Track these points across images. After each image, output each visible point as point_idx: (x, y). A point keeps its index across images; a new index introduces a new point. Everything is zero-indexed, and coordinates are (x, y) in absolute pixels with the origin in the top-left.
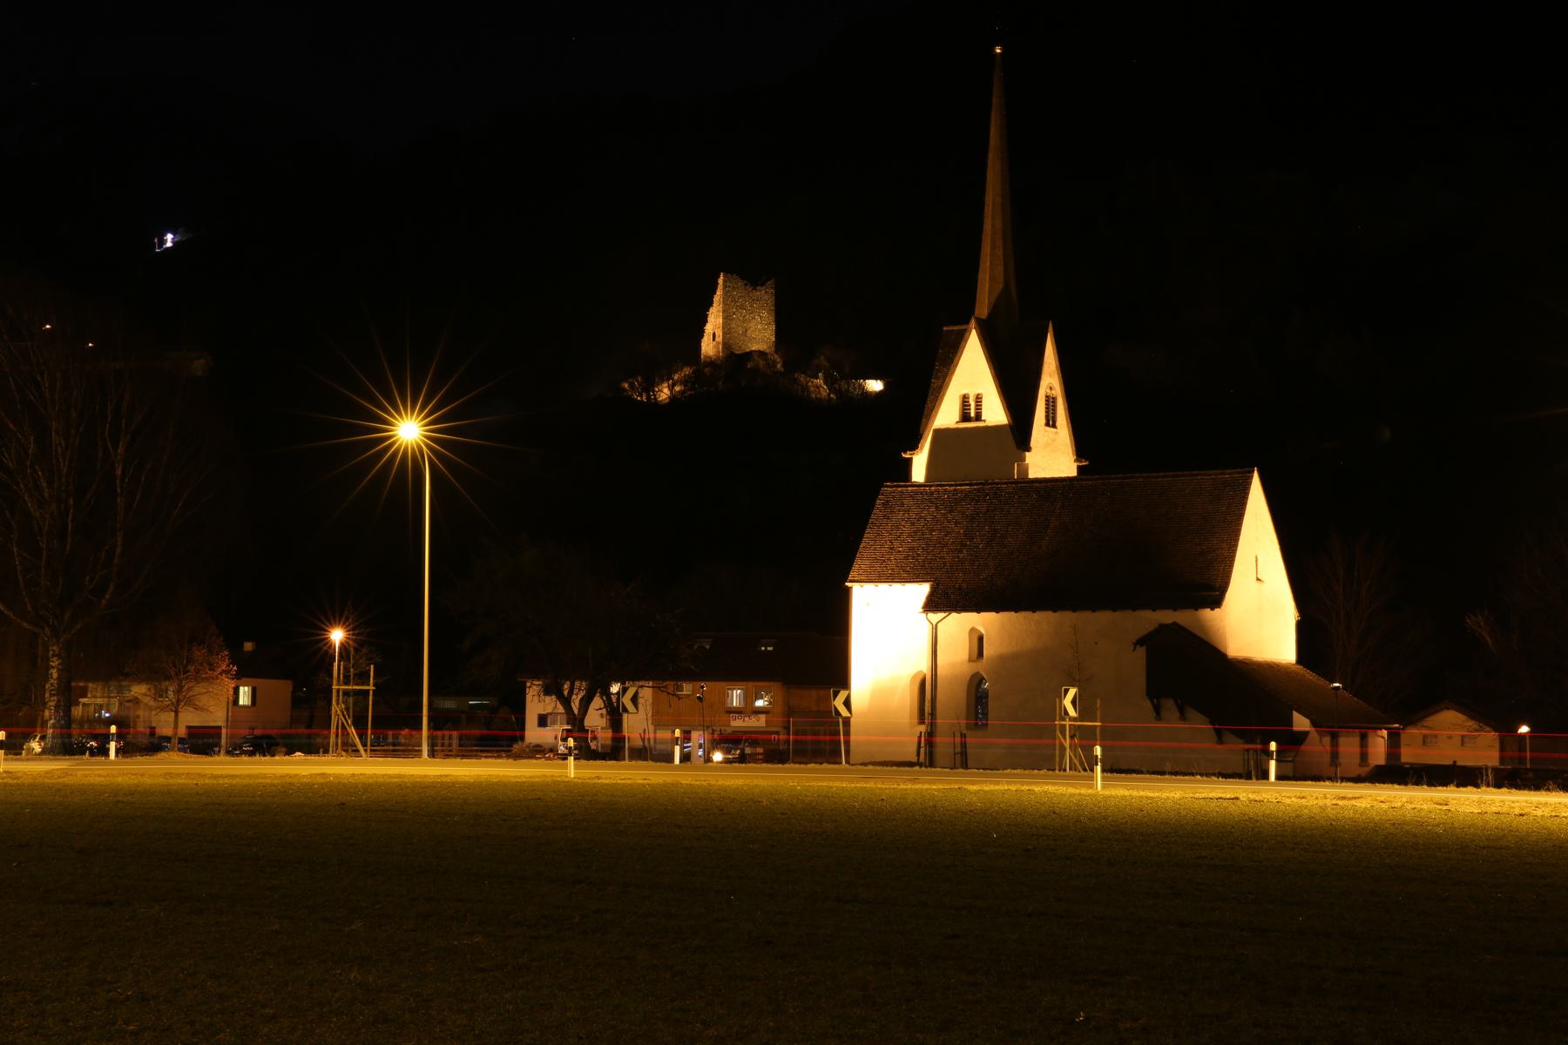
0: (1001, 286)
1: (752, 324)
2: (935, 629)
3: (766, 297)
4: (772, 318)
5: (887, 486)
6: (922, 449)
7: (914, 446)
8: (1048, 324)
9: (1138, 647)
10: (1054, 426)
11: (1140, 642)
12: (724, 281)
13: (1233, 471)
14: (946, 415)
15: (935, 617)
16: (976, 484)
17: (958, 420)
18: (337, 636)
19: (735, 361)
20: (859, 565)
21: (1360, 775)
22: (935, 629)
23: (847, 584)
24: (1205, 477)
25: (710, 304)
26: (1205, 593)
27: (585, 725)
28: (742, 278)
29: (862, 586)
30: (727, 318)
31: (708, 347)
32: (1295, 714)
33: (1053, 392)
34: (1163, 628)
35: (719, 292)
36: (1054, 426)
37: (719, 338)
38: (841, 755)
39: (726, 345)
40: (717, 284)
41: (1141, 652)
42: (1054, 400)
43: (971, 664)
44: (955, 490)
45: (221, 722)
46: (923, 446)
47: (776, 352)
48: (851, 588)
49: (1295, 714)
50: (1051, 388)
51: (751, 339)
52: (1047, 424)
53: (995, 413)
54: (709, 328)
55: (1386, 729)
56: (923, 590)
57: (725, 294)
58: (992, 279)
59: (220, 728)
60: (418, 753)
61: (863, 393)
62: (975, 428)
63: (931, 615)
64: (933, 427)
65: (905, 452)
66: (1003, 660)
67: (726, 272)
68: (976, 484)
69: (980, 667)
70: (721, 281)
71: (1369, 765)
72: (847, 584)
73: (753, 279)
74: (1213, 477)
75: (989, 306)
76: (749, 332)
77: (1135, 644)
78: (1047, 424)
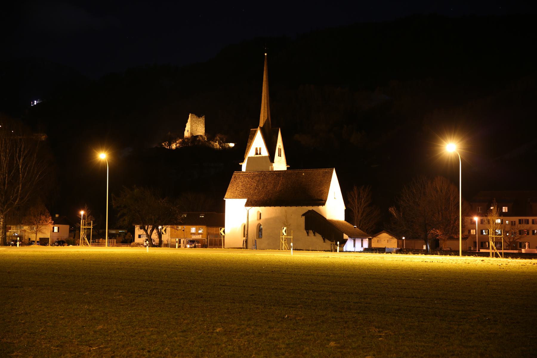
0: (266, 118)
3: (202, 120)
4: (204, 126)
7: (242, 161)
9: (303, 216)
10: (280, 156)
11: (303, 215)
12: (191, 116)
14: (251, 153)
19: (194, 138)
25: (187, 122)
28: (196, 115)
30: (192, 126)
31: (187, 134)
32: (344, 234)
36: (280, 156)
37: (189, 131)
39: (191, 133)
44: (254, 173)
47: (205, 135)
49: (344, 234)
51: (198, 132)
52: (279, 156)
53: (265, 153)
54: (187, 129)
55: (368, 238)
57: (191, 119)
58: (264, 116)
59: (49, 238)
65: (240, 163)
66: (267, 220)
67: (191, 113)
69: (261, 222)
70: (190, 116)
73: (199, 116)
75: (263, 123)
77: (302, 216)
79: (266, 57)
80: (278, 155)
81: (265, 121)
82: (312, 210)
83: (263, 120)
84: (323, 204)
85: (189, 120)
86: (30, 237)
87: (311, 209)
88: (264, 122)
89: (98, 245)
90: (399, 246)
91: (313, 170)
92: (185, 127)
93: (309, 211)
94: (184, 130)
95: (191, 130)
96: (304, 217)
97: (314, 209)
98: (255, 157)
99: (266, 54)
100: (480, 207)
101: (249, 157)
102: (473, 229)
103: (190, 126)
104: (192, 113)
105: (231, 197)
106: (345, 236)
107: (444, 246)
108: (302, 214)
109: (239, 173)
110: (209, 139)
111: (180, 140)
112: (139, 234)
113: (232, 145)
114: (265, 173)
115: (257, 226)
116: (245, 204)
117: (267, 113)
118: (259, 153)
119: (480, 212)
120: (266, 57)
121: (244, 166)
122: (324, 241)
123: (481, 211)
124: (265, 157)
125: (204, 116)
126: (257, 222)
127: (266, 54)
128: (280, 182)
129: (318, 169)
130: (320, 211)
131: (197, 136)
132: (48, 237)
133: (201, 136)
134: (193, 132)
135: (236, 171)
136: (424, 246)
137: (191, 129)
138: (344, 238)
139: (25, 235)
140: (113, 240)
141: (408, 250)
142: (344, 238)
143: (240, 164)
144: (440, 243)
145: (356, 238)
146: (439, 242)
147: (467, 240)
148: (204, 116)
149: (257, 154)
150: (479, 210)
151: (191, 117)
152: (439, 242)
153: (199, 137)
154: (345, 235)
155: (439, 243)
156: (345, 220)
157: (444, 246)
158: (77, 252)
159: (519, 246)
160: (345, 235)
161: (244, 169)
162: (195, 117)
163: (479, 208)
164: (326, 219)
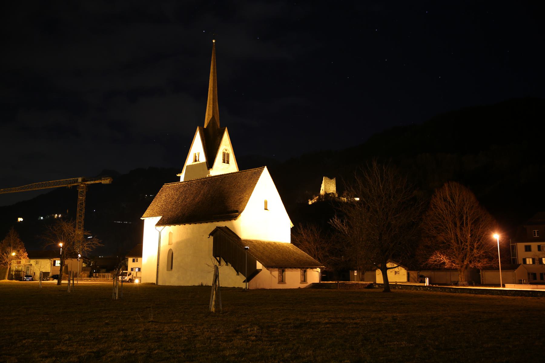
0: (211, 117)
1: (331, 187)
2: (160, 233)
3: (334, 181)
4: (335, 186)
5: (165, 185)
7: (180, 172)
8: (225, 129)
9: (211, 236)
10: (228, 163)
11: (211, 234)
12: (324, 178)
13: (254, 169)
14: (190, 161)
16: (187, 181)
18: (61, 245)
19: (327, 195)
20: (148, 211)
21: (300, 287)
22: (160, 233)
23: (141, 218)
24: (250, 171)
25: (322, 183)
26: (234, 214)
27: (389, 281)
28: (328, 178)
30: (325, 186)
31: (322, 192)
32: (258, 262)
36: (228, 163)
37: (324, 190)
39: (326, 192)
40: (323, 179)
41: (212, 238)
42: (228, 155)
43: (169, 245)
44: (181, 184)
45: (50, 271)
47: (336, 193)
48: (144, 220)
49: (258, 262)
52: (224, 162)
53: (203, 159)
54: (322, 188)
55: (320, 268)
56: (159, 218)
58: (208, 115)
59: (49, 272)
60: (500, 287)
61: (354, 201)
65: (178, 174)
67: (325, 176)
68: (187, 181)
70: (324, 178)
71: (307, 283)
72: (141, 218)
73: (331, 178)
74: (252, 171)
75: (207, 122)
77: (210, 235)
78: (224, 162)
79: (214, 44)
81: (209, 120)
82: (226, 227)
83: (207, 120)
84: (235, 217)
86: (35, 272)
87: (224, 226)
88: (208, 122)
90: (411, 279)
91: (242, 172)
93: (218, 229)
96: (212, 238)
97: (227, 226)
98: (192, 165)
100: (536, 231)
101: (187, 166)
102: (529, 258)
104: (325, 176)
105: (149, 216)
107: (460, 279)
109: (167, 185)
110: (339, 196)
111: (317, 197)
112: (132, 267)
113: (357, 199)
114: (192, 182)
115: (168, 254)
116: (155, 224)
117: (212, 111)
118: (197, 160)
119: (536, 236)
121: (182, 176)
122: (238, 274)
123: (535, 231)
125: (335, 178)
129: (248, 170)
130: (234, 228)
131: (330, 194)
132: (49, 271)
133: (333, 193)
136: (426, 280)
138: (257, 269)
139: (31, 269)
140: (108, 274)
142: (257, 269)
143: (177, 175)
144: (481, 275)
145: (308, 268)
146: (480, 273)
147: (516, 270)
148: (335, 178)
149: (196, 161)
150: (535, 233)
152: (480, 273)
153: (331, 194)
154: (258, 263)
155: (480, 274)
156: (293, 241)
157: (461, 279)
160: (258, 263)
161: (182, 180)
162: (328, 179)
164: (240, 239)
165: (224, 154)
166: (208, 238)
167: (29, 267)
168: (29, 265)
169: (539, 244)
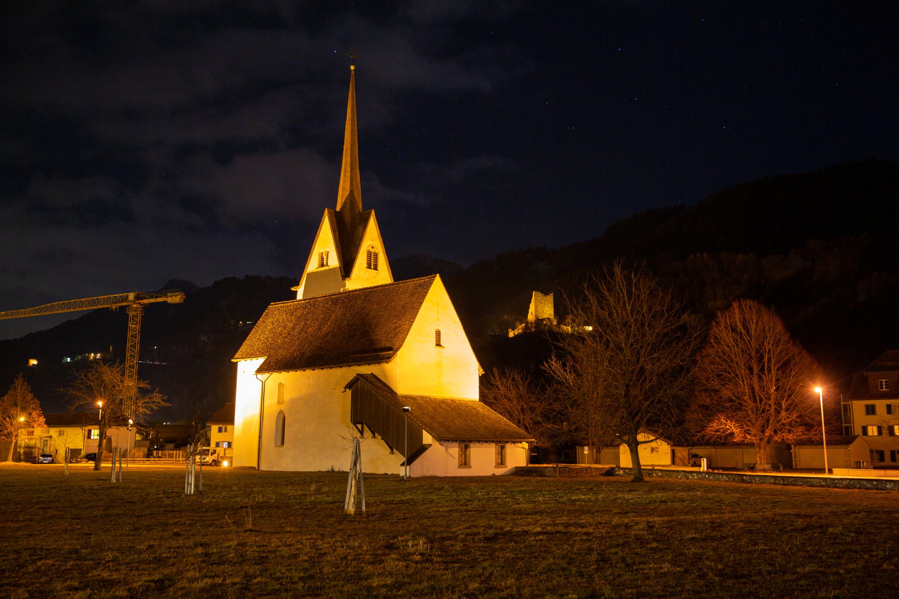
0: (348, 193)
4: (553, 306)
5: (272, 305)
6: (301, 285)
7: (297, 283)
9: (347, 390)
10: (376, 268)
14: (312, 266)
15: (263, 376)
16: (308, 299)
17: (317, 267)
18: (100, 404)
19: (539, 321)
22: (263, 384)
23: (232, 360)
29: (251, 360)
30: (536, 307)
31: (531, 317)
33: (375, 250)
34: (359, 377)
35: (533, 298)
36: (376, 268)
37: (534, 314)
38: (826, 441)
39: (536, 316)
40: (532, 295)
42: (376, 255)
44: (298, 304)
45: (82, 448)
46: (302, 283)
50: (372, 247)
51: (545, 314)
53: (334, 262)
54: (530, 311)
55: (527, 442)
57: (535, 298)
62: (325, 270)
63: (259, 376)
64: (307, 272)
65: (293, 287)
66: (293, 401)
67: (535, 290)
69: (282, 407)
70: (534, 294)
71: (506, 467)
75: (341, 203)
76: (544, 312)
77: (345, 388)
79: (353, 73)
80: (365, 265)
81: (345, 198)
82: (372, 374)
83: (342, 197)
84: (388, 359)
85: (533, 300)
86: (57, 448)
87: (370, 373)
89: (134, 460)
92: (529, 308)
94: (528, 312)
95: (535, 312)
96: (349, 392)
98: (317, 272)
99: (352, 68)
100: (884, 381)
103: (534, 307)
106: (427, 438)
107: (759, 460)
108: (346, 384)
110: (559, 323)
120: (353, 73)
122: (392, 453)
123: (886, 388)
124: (334, 269)
126: (277, 409)
127: (352, 68)
128: (333, 317)
130: (385, 376)
131: (544, 319)
132: (78, 448)
133: (549, 319)
134: (538, 315)
135: (274, 302)
137: (536, 311)
138: (423, 443)
140: (178, 451)
141: (627, 471)
142: (423, 443)
143: (292, 289)
145: (507, 442)
150: (882, 385)
151: (535, 296)
152: (791, 451)
155: (791, 453)
156: (483, 397)
158: (248, 470)
159: (11, 458)
161: (300, 296)
162: (541, 294)
163: (882, 382)
165: (369, 254)
166: (343, 392)
167: (47, 440)
168: (48, 437)
169: (889, 402)
